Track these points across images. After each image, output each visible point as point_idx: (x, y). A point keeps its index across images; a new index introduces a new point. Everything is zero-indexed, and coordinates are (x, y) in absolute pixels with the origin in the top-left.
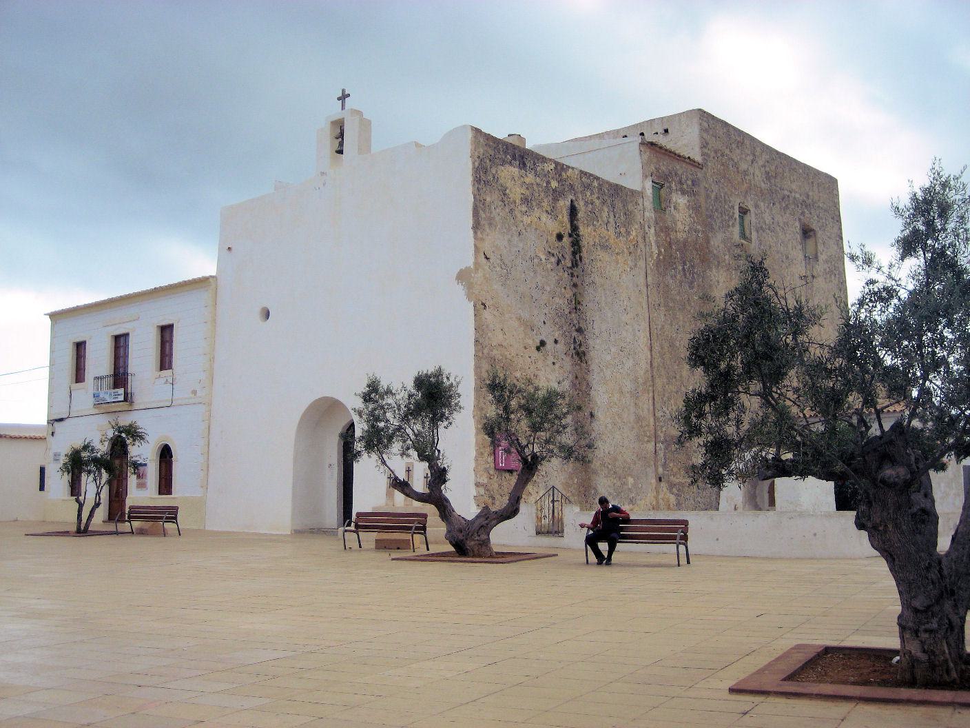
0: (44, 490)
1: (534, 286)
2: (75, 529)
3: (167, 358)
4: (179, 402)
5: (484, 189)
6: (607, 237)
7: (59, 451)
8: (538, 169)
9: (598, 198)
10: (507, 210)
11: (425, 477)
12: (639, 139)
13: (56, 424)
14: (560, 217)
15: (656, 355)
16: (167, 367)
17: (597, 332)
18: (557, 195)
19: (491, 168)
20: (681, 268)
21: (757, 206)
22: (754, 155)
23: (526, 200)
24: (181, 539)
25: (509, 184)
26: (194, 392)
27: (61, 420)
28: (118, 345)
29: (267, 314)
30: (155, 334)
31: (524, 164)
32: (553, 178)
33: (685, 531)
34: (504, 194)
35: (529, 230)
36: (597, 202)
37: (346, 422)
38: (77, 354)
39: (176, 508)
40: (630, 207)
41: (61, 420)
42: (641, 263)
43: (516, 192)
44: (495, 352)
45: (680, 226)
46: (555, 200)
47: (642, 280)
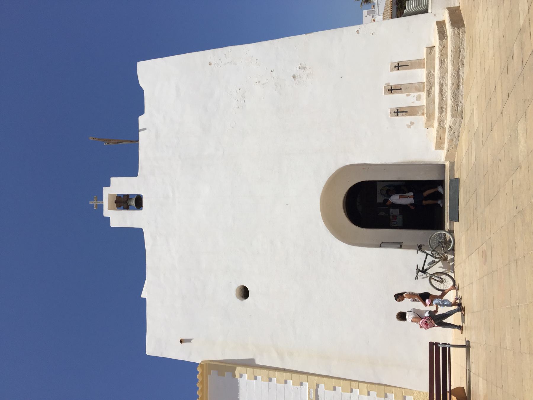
29: (245, 293)
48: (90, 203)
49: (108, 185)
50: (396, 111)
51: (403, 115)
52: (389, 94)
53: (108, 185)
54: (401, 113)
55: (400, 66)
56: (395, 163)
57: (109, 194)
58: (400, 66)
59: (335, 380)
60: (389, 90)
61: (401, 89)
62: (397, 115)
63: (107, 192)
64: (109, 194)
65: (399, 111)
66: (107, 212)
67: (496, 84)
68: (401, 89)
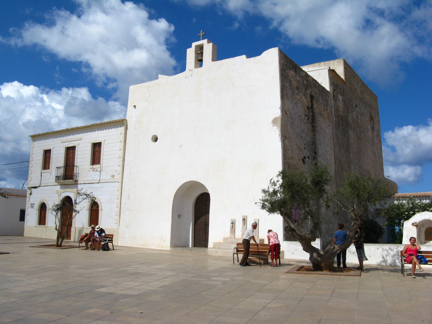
0: (44, 224)
1: (301, 130)
2: (55, 243)
3: (47, 164)
4: (103, 181)
5: (284, 80)
6: (321, 110)
7: (34, 203)
8: (300, 74)
9: (318, 91)
10: (292, 92)
11: (231, 223)
12: (328, 68)
13: (32, 189)
14: (308, 98)
15: (337, 167)
16: (47, 168)
17: (320, 154)
18: (307, 88)
19: (286, 70)
20: (342, 128)
21: (359, 104)
22: (358, 83)
23: (297, 88)
24: (114, 251)
25: (292, 79)
26: (113, 176)
27: (36, 187)
28: (46, 157)
29: (155, 139)
30: (43, 154)
31: (296, 71)
32: (305, 79)
33: (112, 238)
34: (291, 84)
35: (299, 102)
36: (318, 93)
37: (199, 193)
38: (45, 157)
39: (112, 235)
40: (327, 98)
41: (36, 187)
42: (331, 124)
43: (294, 83)
44: (290, 161)
45: (341, 109)
46: (306, 90)
47: (331, 132)
48: (201, 31)
49: (208, 42)
50: (233, 223)
51: (231, 226)
52: (242, 219)
53: (208, 42)
54: (232, 225)
55: (104, 152)
56: (193, 216)
57: (203, 44)
58: (104, 152)
59: (120, 191)
60: (244, 218)
61: (244, 225)
62: (231, 223)
63: (204, 42)
64: (203, 44)
65: (233, 224)
66: (194, 44)
67: (123, 289)
68: (244, 225)
